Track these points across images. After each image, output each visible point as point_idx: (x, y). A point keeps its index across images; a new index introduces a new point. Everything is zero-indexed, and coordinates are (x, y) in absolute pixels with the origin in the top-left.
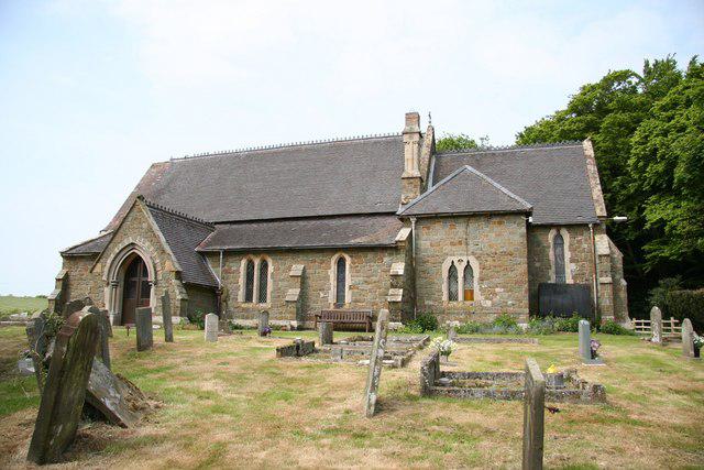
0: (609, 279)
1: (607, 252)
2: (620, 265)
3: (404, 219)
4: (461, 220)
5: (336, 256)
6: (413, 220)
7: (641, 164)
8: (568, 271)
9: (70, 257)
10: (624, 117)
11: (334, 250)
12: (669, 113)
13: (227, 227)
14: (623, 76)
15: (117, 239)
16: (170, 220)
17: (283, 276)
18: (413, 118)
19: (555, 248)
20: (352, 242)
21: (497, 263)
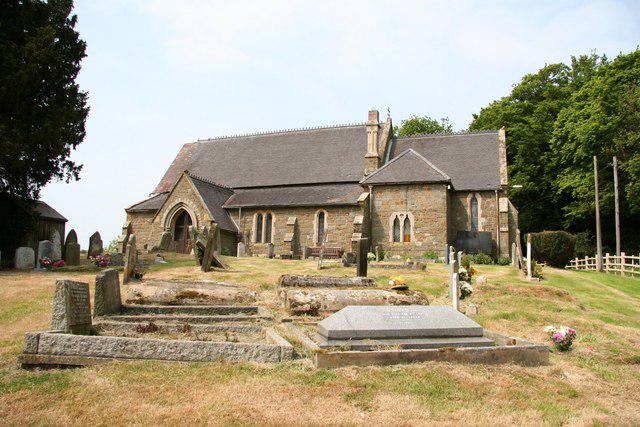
0: (507, 229)
1: (506, 209)
2: (516, 219)
3: (365, 187)
6: (370, 187)
7: (559, 143)
8: (480, 223)
9: (133, 212)
10: (553, 104)
11: (317, 207)
12: (581, 103)
13: (242, 191)
14: (555, 69)
15: (170, 199)
16: (203, 185)
17: (282, 226)
18: (374, 114)
19: (471, 207)
20: (329, 202)
21: (427, 217)
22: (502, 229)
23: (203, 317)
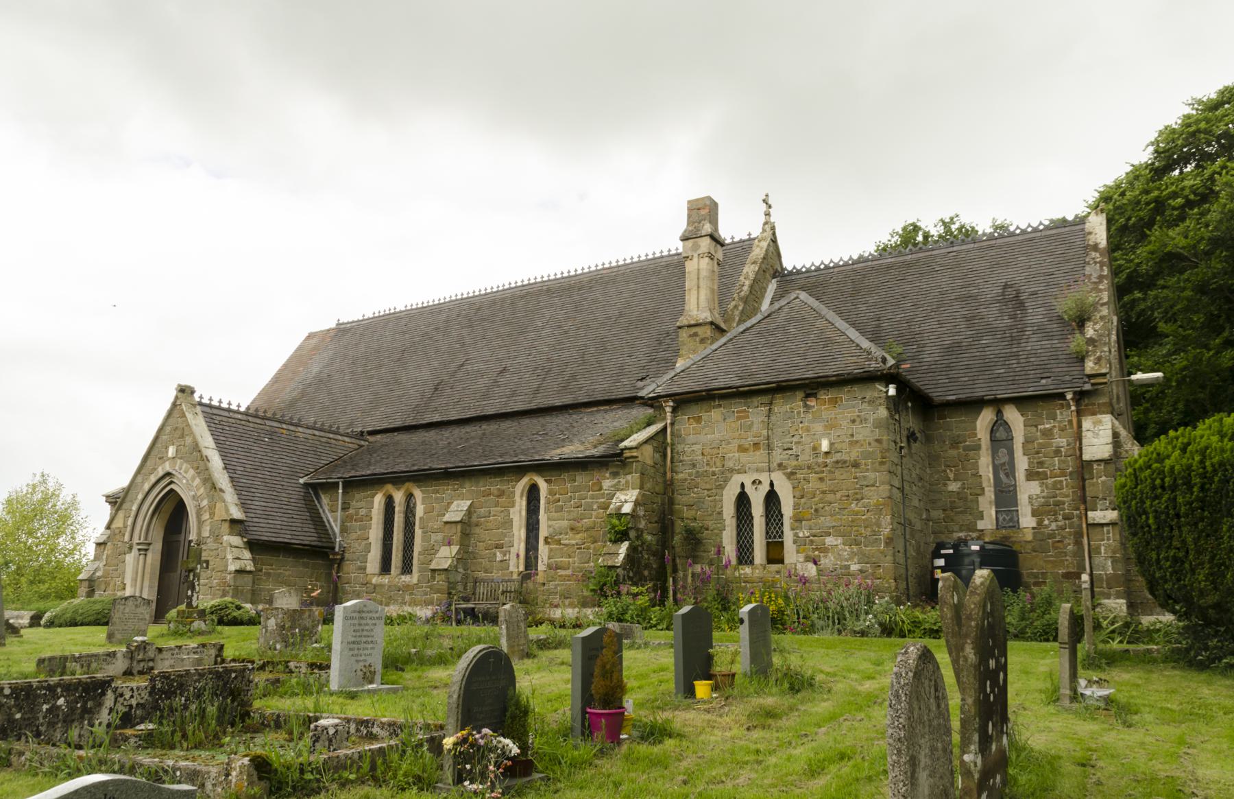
4: (756, 400)
5: (524, 482)
6: (668, 406)
8: (1023, 498)
11: (520, 470)
22: (1097, 516)
23: (671, 588)
